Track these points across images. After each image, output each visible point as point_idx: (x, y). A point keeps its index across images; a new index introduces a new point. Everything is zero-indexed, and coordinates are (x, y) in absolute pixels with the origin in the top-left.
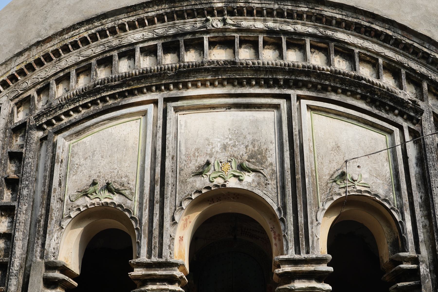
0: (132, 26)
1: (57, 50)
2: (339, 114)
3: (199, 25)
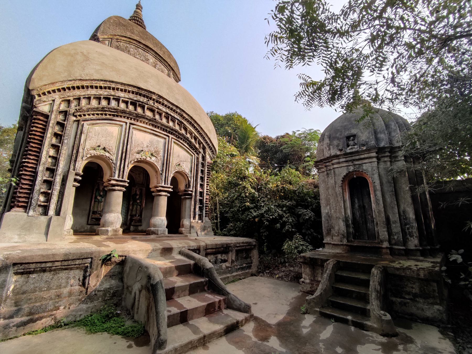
1: (88, 86)
3: (145, 101)
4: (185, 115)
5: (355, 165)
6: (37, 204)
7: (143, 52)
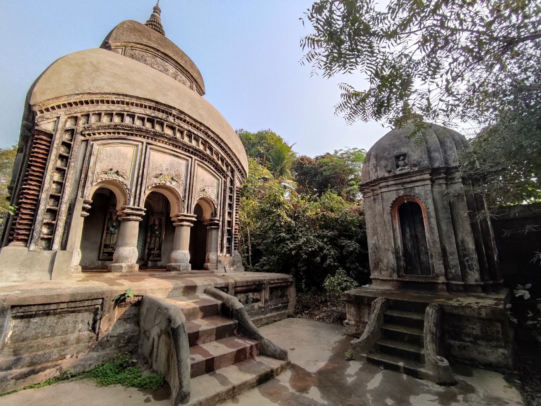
0: (137, 105)
1: (98, 101)
2: (206, 169)
3: (164, 117)
4: (210, 133)
5: (405, 189)
6: (39, 237)
7: (161, 61)
